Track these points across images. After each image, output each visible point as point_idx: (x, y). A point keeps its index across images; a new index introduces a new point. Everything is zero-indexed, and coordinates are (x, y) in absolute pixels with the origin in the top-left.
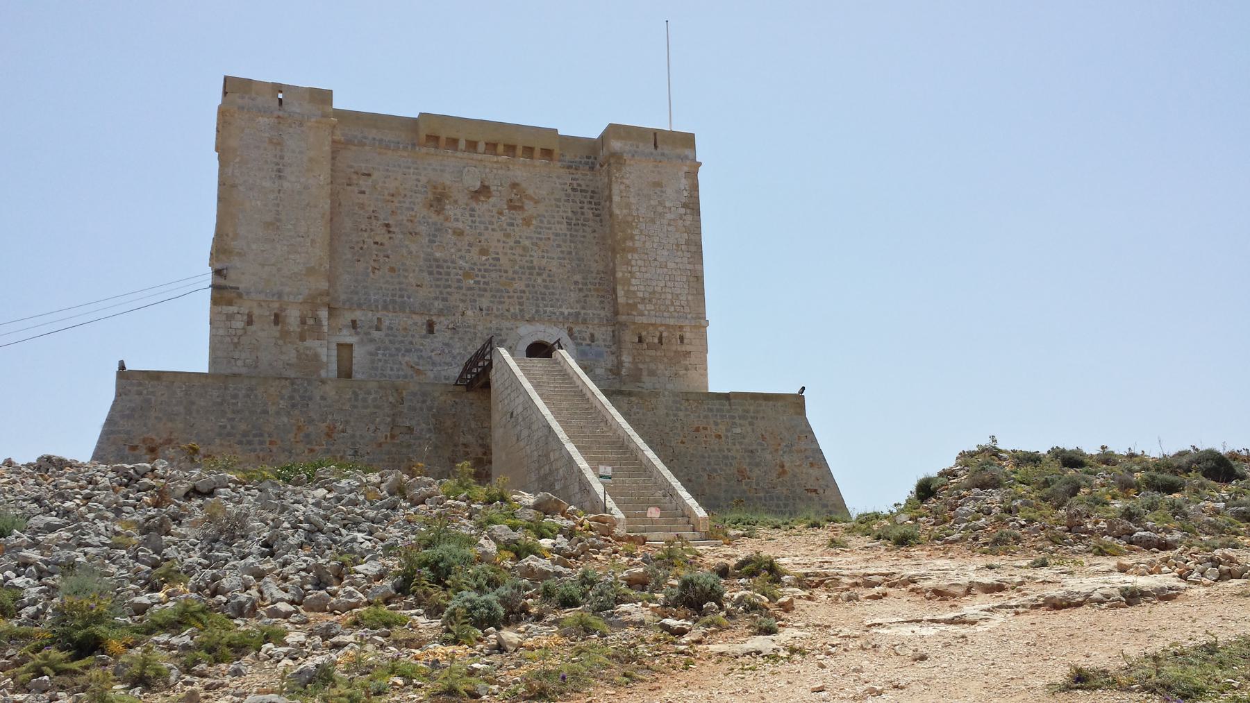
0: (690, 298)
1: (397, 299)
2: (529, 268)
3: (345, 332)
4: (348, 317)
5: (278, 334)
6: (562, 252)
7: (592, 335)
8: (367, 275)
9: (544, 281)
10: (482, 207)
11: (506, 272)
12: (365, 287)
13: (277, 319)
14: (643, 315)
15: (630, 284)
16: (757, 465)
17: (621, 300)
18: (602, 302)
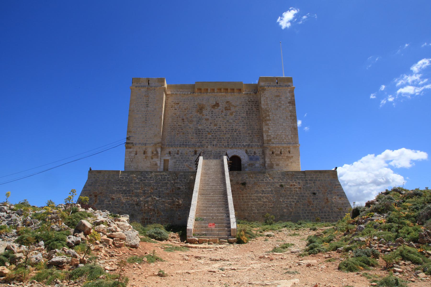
0: (292, 136)
1: (184, 143)
2: (231, 130)
3: (166, 155)
4: (167, 150)
5: (144, 157)
6: (244, 123)
7: (255, 152)
8: (175, 136)
9: (237, 134)
10: (216, 110)
11: (223, 131)
12: (174, 140)
13: (145, 153)
14: (273, 143)
15: (268, 132)
16: (317, 199)
17: (265, 138)
18: (258, 140)
